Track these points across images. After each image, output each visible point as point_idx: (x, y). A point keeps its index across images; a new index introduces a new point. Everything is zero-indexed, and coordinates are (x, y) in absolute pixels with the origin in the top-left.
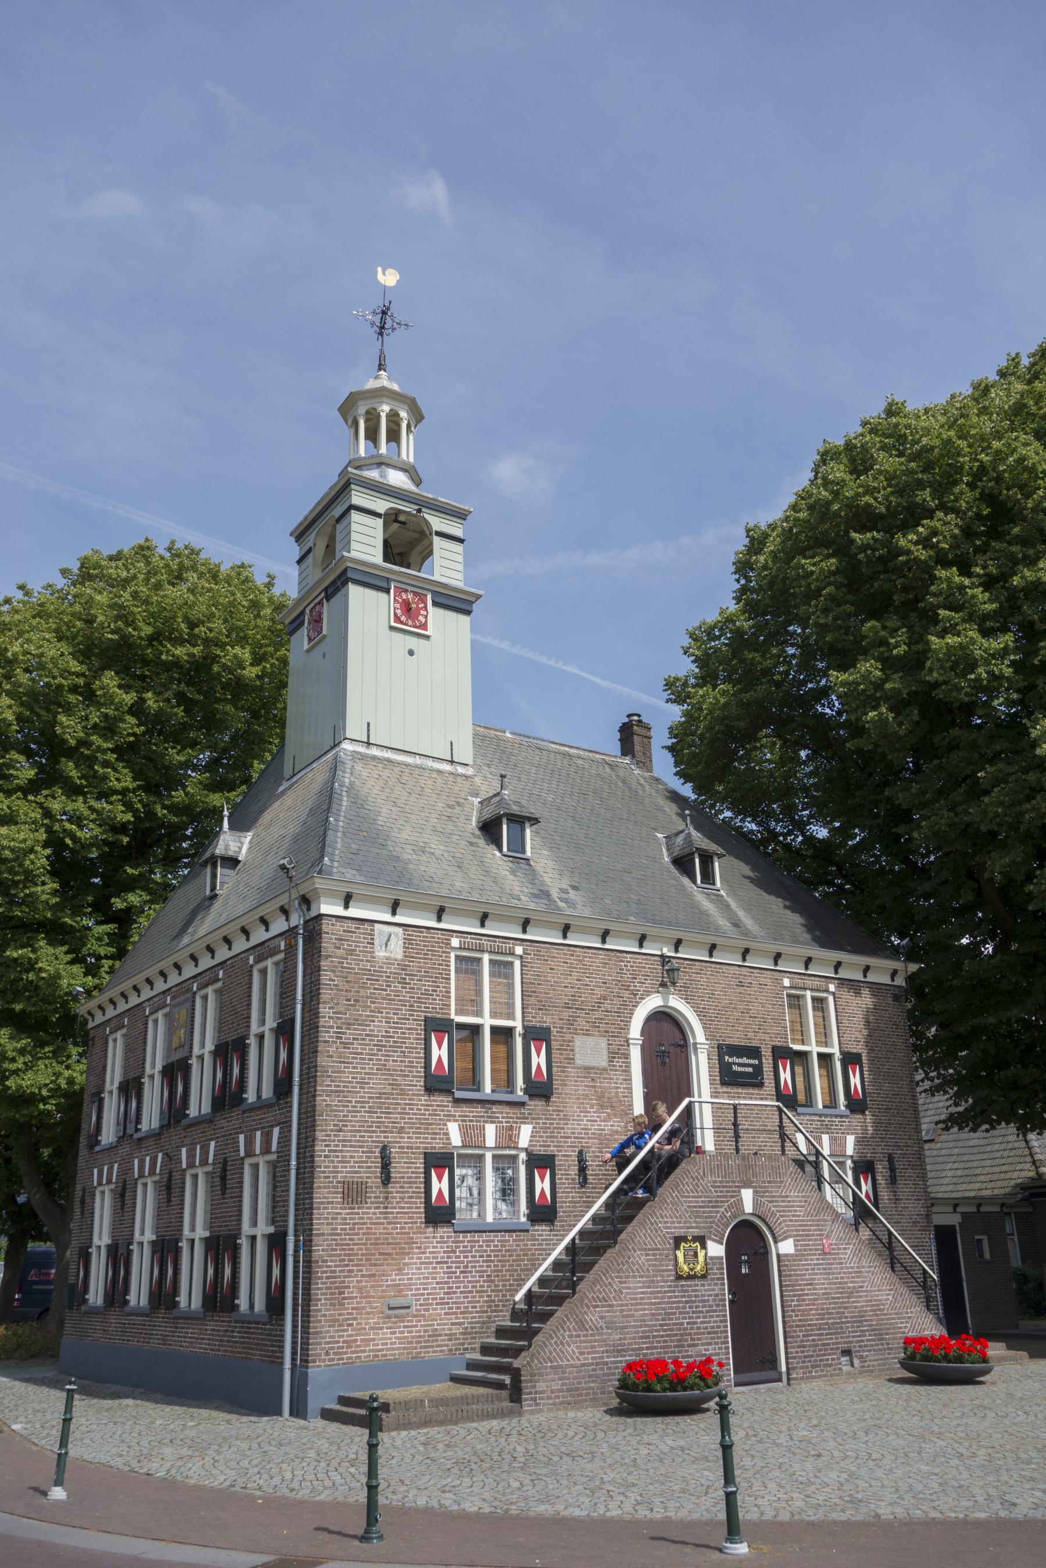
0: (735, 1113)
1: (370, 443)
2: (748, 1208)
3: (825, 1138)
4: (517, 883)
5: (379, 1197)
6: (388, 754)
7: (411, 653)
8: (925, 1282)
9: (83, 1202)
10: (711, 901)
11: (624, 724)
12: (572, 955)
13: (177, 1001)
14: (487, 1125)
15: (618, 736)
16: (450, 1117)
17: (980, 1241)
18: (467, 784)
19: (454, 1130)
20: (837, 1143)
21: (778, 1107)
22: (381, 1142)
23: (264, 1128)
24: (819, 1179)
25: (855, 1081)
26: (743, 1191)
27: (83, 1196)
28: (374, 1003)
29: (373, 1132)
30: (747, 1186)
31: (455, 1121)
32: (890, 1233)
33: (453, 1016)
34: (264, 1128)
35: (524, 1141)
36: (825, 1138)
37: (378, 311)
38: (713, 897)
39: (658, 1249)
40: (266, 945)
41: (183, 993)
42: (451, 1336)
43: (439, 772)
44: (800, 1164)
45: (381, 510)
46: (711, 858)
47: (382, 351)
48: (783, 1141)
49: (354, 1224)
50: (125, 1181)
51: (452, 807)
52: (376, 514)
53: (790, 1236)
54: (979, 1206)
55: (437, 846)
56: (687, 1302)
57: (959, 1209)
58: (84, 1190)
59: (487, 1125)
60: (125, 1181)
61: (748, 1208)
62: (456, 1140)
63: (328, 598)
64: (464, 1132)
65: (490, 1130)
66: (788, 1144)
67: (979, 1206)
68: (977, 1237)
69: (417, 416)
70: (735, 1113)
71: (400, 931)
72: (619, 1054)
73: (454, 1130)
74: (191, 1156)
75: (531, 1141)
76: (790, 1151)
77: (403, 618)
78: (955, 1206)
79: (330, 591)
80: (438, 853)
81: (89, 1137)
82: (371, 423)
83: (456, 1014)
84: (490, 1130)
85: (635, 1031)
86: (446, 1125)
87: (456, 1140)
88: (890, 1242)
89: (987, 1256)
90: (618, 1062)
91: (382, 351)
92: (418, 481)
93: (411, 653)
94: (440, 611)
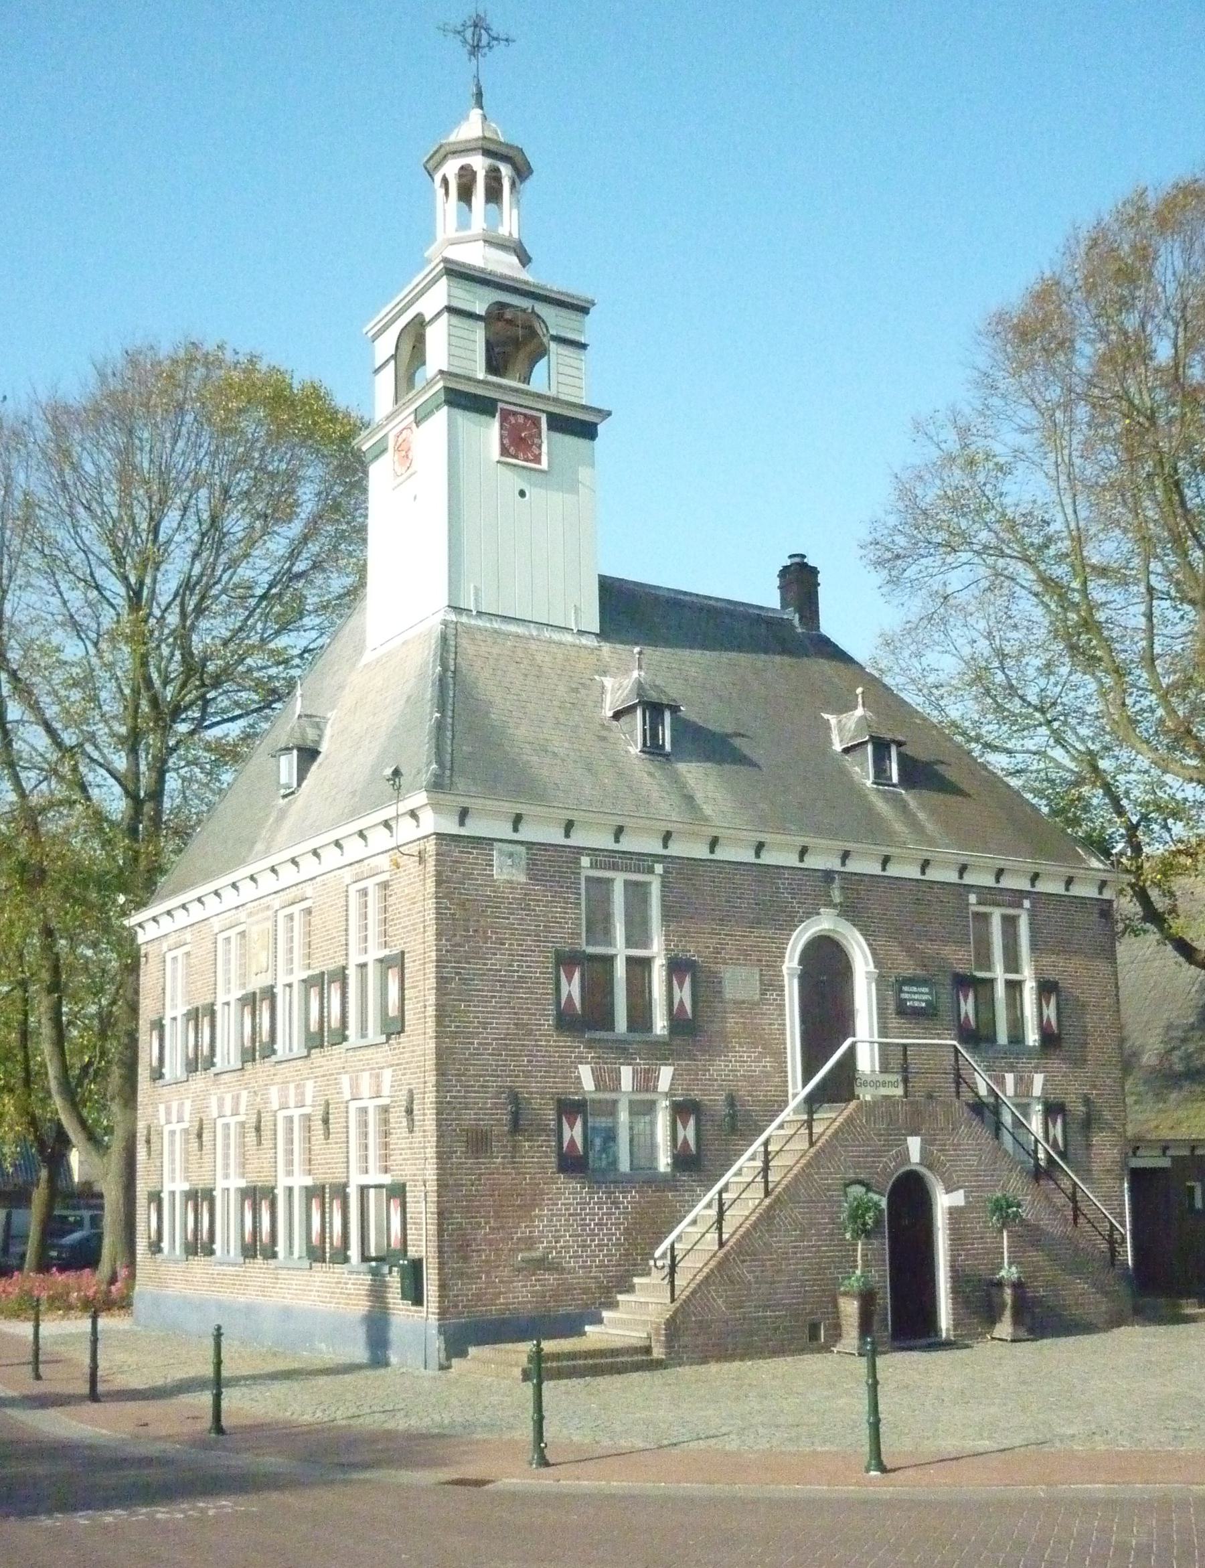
0: (905, 1055)
1: (463, 204)
2: (915, 1156)
3: (1010, 1078)
4: (656, 787)
5: (506, 1146)
6: (390, 315)
7: (522, 494)
8: (1111, 1236)
9: (148, 1142)
10: (887, 800)
11: (785, 568)
12: (720, 873)
13: (254, 918)
14: (622, 1068)
15: (777, 582)
16: (581, 1060)
17: (1192, 1189)
18: (592, 659)
19: (585, 1073)
20: (1023, 1084)
21: (955, 1046)
22: (508, 1087)
23: (372, 1069)
24: (998, 1126)
25: (1051, 1012)
26: (909, 1139)
27: (149, 1134)
28: (497, 933)
29: (498, 1076)
30: (914, 1133)
31: (587, 1063)
32: (1075, 1185)
33: (584, 947)
34: (372, 1069)
35: (1037, 1090)
36: (1010, 1078)
37: (469, 23)
38: (889, 796)
39: (813, 1202)
40: (366, 862)
41: (262, 910)
42: (586, 1291)
43: (560, 643)
44: (978, 1108)
45: (480, 308)
46: (888, 747)
47: (477, 78)
48: (958, 1084)
49: (481, 1174)
50: (201, 1120)
51: (576, 690)
52: (478, 318)
53: (960, 1188)
54: (1193, 1148)
55: (559, 744)
56: (843, 1256)
57: (1169, 1153)
58: (149, 1128)
59: (622, 1068)
60: (201, 1120)
61: (915, 1156)
62: (588, 1084)
63: (418, 423)
64: (598, 1080)
65: (626, 1073)
66: (964, 1088)
67: (1193, 1148)
68: (1189, 1184)
69: (522, 171)
70: (905, 1055)
71: (522, 849)
72: (772, 985)
73: (585, 1073)
74: (284, 1095)
75: (672, 1084)
76: (967, 1096)
77: (512, 450)
78: (1165, 1149)
79: (421, 414)
80: (561, 752)
81: (152, 1070)
82: (464, 180)
83: (587, 943)
84: (626, 1073)
85: (791, 963)
86: (576, 1068)
87: (588, 1084)
88: (1074, 1194)
89: (1199, 1204)
90: (771, 996)
91: (477, 78)
92: (525, 259)
93: (522, 494)
94: (558, 437)
